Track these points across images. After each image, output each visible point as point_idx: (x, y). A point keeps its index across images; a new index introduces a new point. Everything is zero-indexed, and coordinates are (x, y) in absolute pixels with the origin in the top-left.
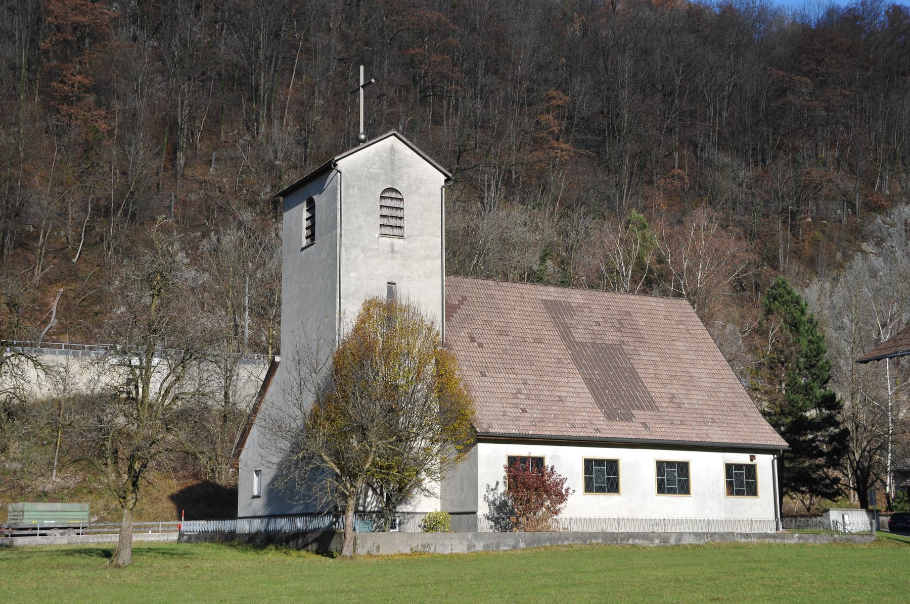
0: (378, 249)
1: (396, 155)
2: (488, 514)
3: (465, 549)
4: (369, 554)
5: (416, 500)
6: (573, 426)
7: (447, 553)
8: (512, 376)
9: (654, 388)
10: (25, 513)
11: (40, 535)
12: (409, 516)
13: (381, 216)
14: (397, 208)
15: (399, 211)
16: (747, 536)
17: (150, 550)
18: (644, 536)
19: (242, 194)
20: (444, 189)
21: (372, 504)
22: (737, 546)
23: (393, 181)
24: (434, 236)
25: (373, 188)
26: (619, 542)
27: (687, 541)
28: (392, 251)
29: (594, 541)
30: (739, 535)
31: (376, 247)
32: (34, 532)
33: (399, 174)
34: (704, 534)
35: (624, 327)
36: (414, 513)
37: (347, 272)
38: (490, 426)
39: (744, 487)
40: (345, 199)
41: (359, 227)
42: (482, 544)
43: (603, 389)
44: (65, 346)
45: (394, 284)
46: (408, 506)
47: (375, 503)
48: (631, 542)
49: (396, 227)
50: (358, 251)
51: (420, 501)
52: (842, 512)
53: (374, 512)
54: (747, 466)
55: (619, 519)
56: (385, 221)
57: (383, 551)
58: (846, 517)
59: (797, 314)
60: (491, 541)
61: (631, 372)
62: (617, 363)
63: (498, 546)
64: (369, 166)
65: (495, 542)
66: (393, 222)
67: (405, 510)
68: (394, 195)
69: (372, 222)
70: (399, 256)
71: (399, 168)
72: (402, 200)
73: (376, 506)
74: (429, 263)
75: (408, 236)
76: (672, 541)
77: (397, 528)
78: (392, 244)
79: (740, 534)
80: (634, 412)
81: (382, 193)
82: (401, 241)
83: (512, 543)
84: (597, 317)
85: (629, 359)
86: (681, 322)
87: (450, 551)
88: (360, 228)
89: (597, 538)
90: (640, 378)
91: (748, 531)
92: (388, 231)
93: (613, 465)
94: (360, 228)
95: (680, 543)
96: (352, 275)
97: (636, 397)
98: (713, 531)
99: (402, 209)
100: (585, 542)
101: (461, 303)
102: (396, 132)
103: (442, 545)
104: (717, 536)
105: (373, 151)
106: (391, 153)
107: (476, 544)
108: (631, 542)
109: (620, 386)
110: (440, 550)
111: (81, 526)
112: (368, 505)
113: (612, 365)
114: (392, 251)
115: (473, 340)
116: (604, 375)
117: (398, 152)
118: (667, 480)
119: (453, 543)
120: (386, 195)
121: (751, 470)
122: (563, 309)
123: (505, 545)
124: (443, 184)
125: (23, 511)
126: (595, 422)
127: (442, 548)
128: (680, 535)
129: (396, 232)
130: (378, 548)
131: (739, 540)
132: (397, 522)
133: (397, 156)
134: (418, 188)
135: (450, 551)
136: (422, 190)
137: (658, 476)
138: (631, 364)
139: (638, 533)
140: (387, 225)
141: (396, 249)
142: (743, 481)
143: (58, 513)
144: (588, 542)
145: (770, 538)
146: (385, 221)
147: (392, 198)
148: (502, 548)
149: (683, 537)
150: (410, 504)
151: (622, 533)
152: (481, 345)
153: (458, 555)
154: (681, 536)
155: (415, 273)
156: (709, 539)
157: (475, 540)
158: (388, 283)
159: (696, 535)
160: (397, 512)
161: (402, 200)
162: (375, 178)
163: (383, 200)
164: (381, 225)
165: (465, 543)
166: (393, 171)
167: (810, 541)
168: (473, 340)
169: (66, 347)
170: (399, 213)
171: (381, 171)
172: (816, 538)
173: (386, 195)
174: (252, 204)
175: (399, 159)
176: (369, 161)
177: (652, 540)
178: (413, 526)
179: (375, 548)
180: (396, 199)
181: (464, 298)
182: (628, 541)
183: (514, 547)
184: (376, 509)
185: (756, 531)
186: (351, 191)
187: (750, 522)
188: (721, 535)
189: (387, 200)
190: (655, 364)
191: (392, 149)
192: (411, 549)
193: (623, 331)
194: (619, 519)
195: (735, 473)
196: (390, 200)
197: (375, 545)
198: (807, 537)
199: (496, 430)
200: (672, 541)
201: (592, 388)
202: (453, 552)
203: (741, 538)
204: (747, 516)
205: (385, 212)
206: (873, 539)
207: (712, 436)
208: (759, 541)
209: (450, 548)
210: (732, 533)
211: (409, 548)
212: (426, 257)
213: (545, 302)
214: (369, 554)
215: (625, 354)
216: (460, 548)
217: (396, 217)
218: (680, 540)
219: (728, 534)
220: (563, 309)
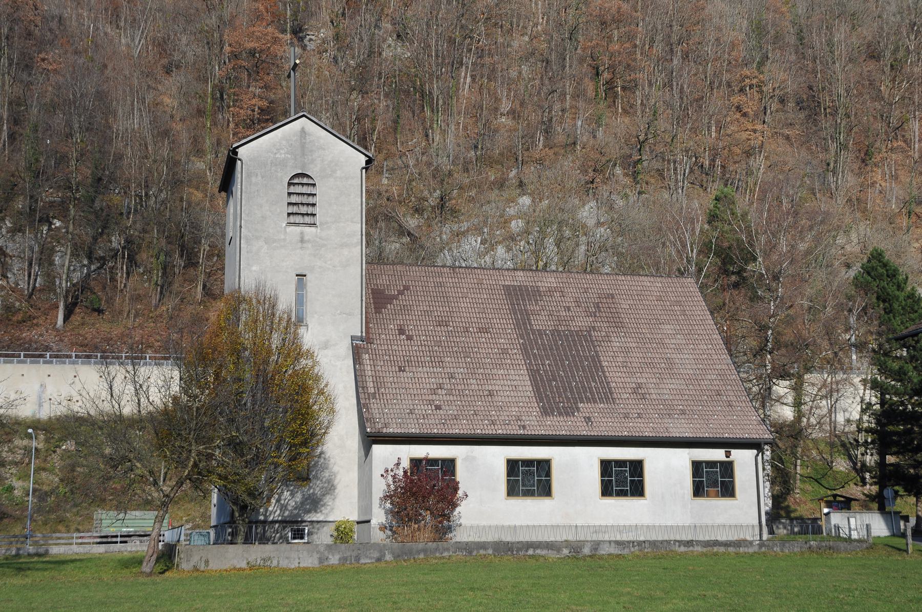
0: (284, 240)
1: (307, 137)
2: (384, 522)
4: (196, 569)
5: (328, 507)
6: (493, 423)
7: (293, 567)
8: (439, 370)
9: (616, 377)
10: (103, 521)
11: (121, 542)
12: (318, 526)
13: (289, 204)
14: (309, 195)
15: (311, 198)
16: (689, 543)
17: (73, 561)
18: (549, 546)
19: (410, 201)
20: (364, 171)
21: (275, 513)
24: (352, 222)
25: (279, 175)
26: (515, 553)
27: (605, 550)
28: (302, 241)
29: (482, 552)
30: (677, 544)
31: (283, 237)
32: (114, 540)
33: (310, 158)
34: (629, 542)
35: (600, 311)
36: (326, 522)
37: (249, 265)
38: (386, 425)
39: (627, 487)
40: (246, 188)
41: (263, 217)
42: (337, 557)
43: (550, 381)
44: (50, 355)
45: (305, 276)
46: (319, 515)
47: (278, 512)
48: (531, 552)
49: (307, 214)
51: (332, 509)
52: (847, 515)
53: (277, 522)
54: (722, 463)
55: (576, 526)
56: (295, 209)
57: (213, 565)
58: (852, 521)
59: (892, 289)
60: (348, 554)
61: (593, 361)
62: (577, 351)
63: (358, 559)
64: (275, 151)
65: (354, 554)
66: (304, 210)
67: (315, 519)
68: (305, 180)
69: (278, 210)
70: (310, 245)
71: (311, 151)
72: (314, 185)
73: (279, 515)
74: (345, 252)
75: (321, 224)
76: (586, 551)
77: (306, 538)
78: (302, 233)
79: (678, 541)
80: (581, 405)
81: (290, 180)
82: (313, 229)
84: (569, 301)
85: (594, 347)
86: (678, 303)
87: (297, 565)
88: (264, 218)
89: (485, 549)
90: (602, 367)
91: (689, 538)
92: (298, 219)
93: (544, 466)
94: (264, 218)
95: (597, 553)
96: (254, 268)
97: (590, 388)
98: (642, 538)
99: (314, 195)
100: (470, 553)
101: (401, 293)
102: (305, 113)
103: (287, 558)
104: (647, 545)
105: (280, 135)
106: (301, 136)
107: (330, 557)
108: (531, 552)
109: (573, 376)
110: (284, 564)
111: (119, 534)
112: (270, 514)
113: (571, 353)
114: (302, 241)
115: (401, 331)
116: (557, 365)
117: (309, 135)
118: (616, 481)
119: (301, 556)
120: (296, 181)
121: (727, 468)
122: (528, 295)
123: (367, 557)
124: (364, 165)
125: (101, 520)
126: (524, 418)
127: (286, 561)
128: (597, 545)
129: (307, 219)
130: (207, 562)
131: (677, 548)
132: (306, 531)
133: (308, 139)
135: (297, 565)
136: (339, 173)
137: (508, 476)
138: (596, 352)
139: (540, 542)
140: (296, 214)
141: (306, 238)
142: (718, 481)
143: (137, 521)
144: (475, 553)
145: (720, 546)
146: (295, 209)
147: (303, 184)
148: (362, 561)
149: (601, 546)
150: (321, 511)
151: (518, 542)
152: (410, 338)
153: (305, 569)
154: (598, 544)
155: (329, 262)
156: (637, 548)
157: (329, 553)
158: (297, 275)
159: (618, 543)
160: (305, 521)
161: (314, 185)
162: (283, 164)
163: (292, 187)
164: (289, 214)
165: (316, 556)
166: (303, 154)
167: (775, 549)
168: (401, 331)
169: (150, 358)
170: (311, 200)
171: (289, 156)
172: (784, 545)
173: (296, 181)
174: (418, 211)
175: (310, 142)
176: (275, 145)
177: (559, 550)
178: (324, 537)
179: (203, 562)
180: (308, 184)
181: (406, 288)
182: (527, 551)
183: (379, 560)
184: (280, 518)
185: (701, 538)
186: (254, 179)
187: (574, 529)
188: (653, 544)
189: (297, 186)
190: (626, 351)
191: (303, 131)
192: (248, 563)
193: (598, 315)
194: (576, 526)
195: (707, 472)
196: (300, 186)
197: (203, 559)
198: (771, 544)
199: (393, 429)
200: (586, 551)
201: (535, 380)
202: (301, 565)
203: (679, 546)
204: (720, 520)
205: (294, 199)
206: (865, 546)
207: (671, 430)
208: (705, 550)
209: (297, 561)
210: (668, 542)
211: (245, 562)
213: (507, 288)
214: (196, 569)
215: (592, 341)
216: (310, 561)
217: (308, 205)
218: (596, 549)
219: (662, 542)
220: (528, 295)
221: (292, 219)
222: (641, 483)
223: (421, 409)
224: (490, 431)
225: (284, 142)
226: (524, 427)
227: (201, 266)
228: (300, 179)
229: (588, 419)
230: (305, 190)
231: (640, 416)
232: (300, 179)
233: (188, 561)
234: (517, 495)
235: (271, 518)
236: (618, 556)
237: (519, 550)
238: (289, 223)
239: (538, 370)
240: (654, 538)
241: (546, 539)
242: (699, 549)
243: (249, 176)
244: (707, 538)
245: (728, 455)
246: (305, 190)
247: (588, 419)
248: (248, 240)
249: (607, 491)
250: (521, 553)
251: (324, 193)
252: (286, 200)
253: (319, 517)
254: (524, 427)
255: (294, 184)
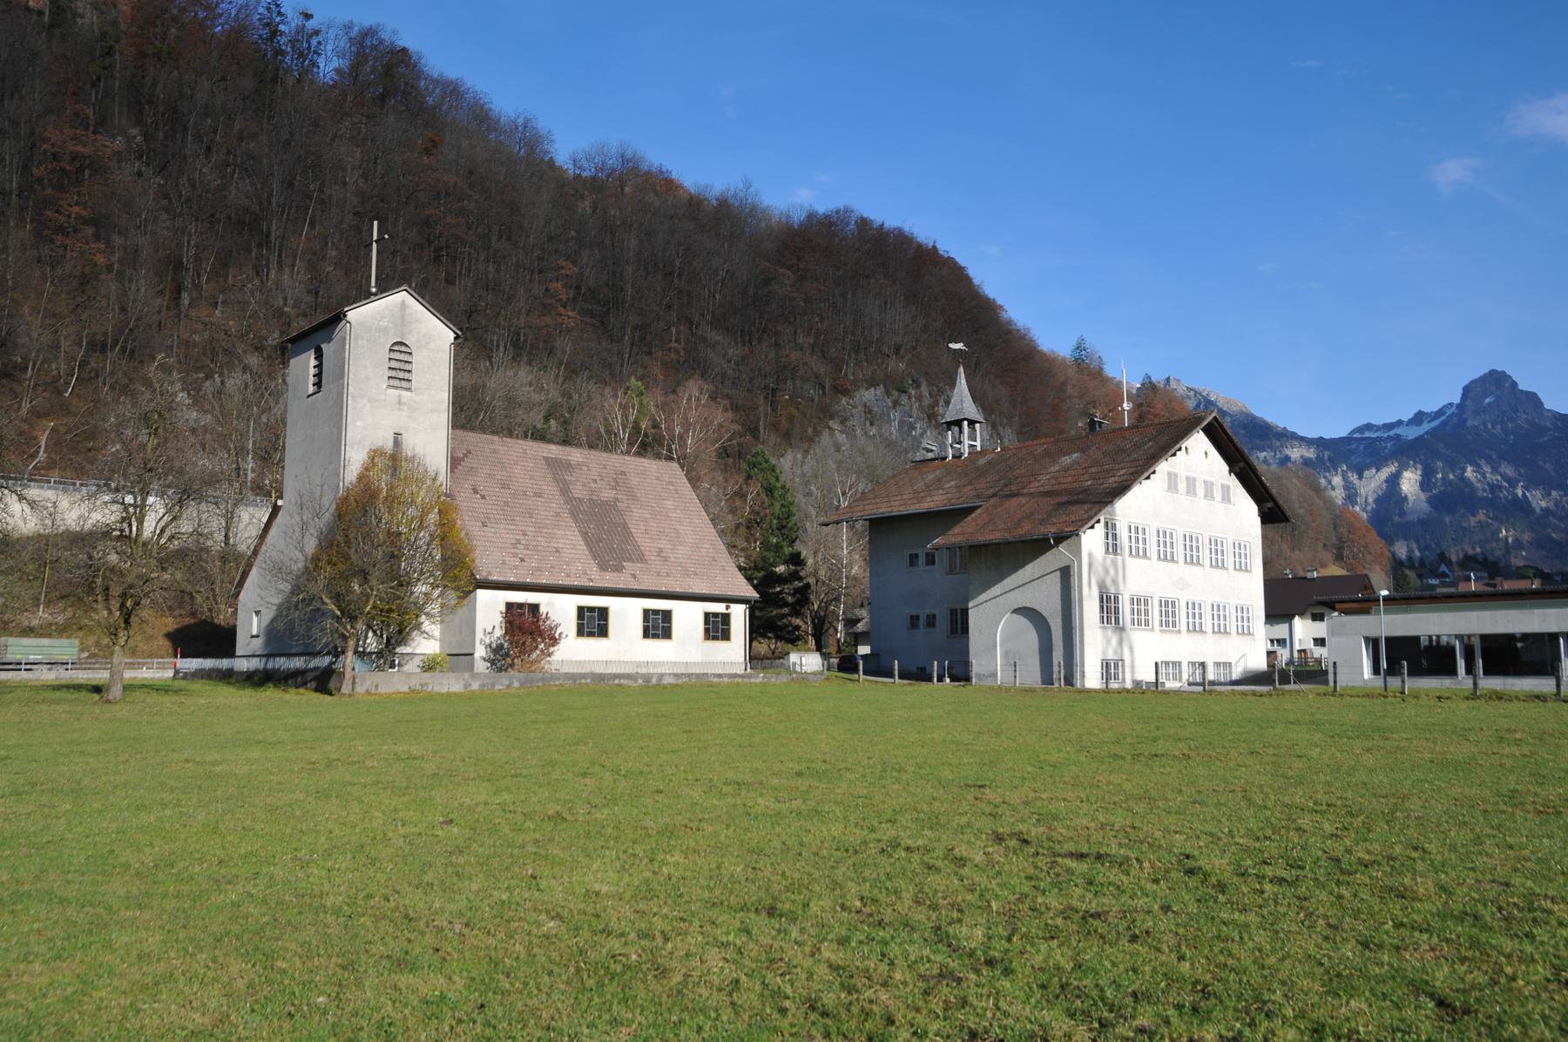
0: (385, 400)
3: (462, 687)
6: (568, 575)
9: (645, 543)
14: (406, 362)
16: (720, 676)
22: (710, 685)
23: (403, 336)
27: (667, 680)
28: (400, 403)
29: (583, 681)
38: (490, 573)
48: (617, 682)
50: (365, 401)
54: (723, 614)
66: (401, 375)
68: (403, 349)
72: (410, 353)
75: (416, 389)
76: (654, 681)
78: (399, 396)
81: (393, 345)
83: (507, 682)
86: (671, 483)
89: (586, 678)
92: (396, 383)
93: (603, 612)
100: (575, 681)
105: (383, 305)
108: (617, 682)
110: (437, 689)
114: (400, 403)
115: (476, 491)
120: (395, 348)
121: (726, 618)
128: (661, 676)
129: (404, 384)
130: (377, 686)
134: (428, 343)
136: (432, 346)
141: (403, 401)
147: (401, 352)
148: (497, 687)
152: (483, 497)
159: (676, 675)
161: (410, 353)
162: (385, 330)
165: (462, 683)
166: (403, 325)
168: (476, 491)
169: (55, 482)
170: (407, 367)
173: (395, 348)
177: (636, 680)
180: (405, 352)
183: (508, 686)
186: (360, 342)
188: (698, 676)
199: (495, 578)
200: (654, 681)
204: (720, 658)
212: (433, 411)
213: (546, 459)
221: (392, 382)
222: (729, 630)
223: (510, 561)
224: (562, 581)
225: (387, 312)
226: (591, 580)
227: (30, 380)
228: (399, 346)
229: (634, 576)
230: (402, 357)
231: (668, 575)
232: (399, 346)
233: (362, 685)
234: (583, 636)
235: (368, 650)
236: (677, 685)
237: (609, 680)
238: (390, 386)
239: (587, 533)
240: (698, 672)
241: (627, 671)
242: (726, 680)
243: (357, 338)
244: (731, 672)
245: (728, 608)
246: (402, 357)
247: (634, 576)
248: (353, 397)
249: (647, 634)
250: (610, 682)
251: (419, 360)
252: (388, 365)
253: (407, 650)
254: (591, 580)
255: (394, 351)
